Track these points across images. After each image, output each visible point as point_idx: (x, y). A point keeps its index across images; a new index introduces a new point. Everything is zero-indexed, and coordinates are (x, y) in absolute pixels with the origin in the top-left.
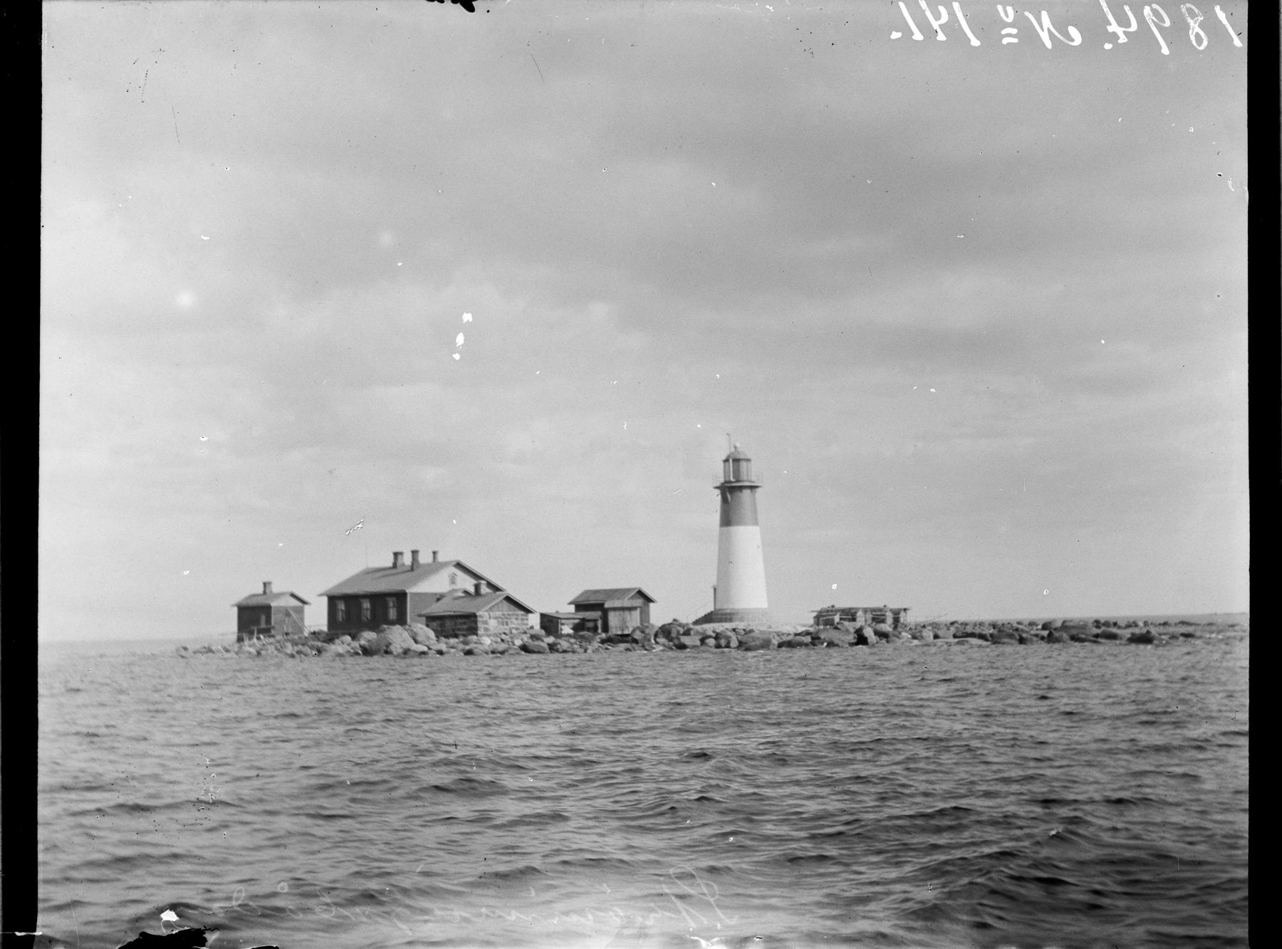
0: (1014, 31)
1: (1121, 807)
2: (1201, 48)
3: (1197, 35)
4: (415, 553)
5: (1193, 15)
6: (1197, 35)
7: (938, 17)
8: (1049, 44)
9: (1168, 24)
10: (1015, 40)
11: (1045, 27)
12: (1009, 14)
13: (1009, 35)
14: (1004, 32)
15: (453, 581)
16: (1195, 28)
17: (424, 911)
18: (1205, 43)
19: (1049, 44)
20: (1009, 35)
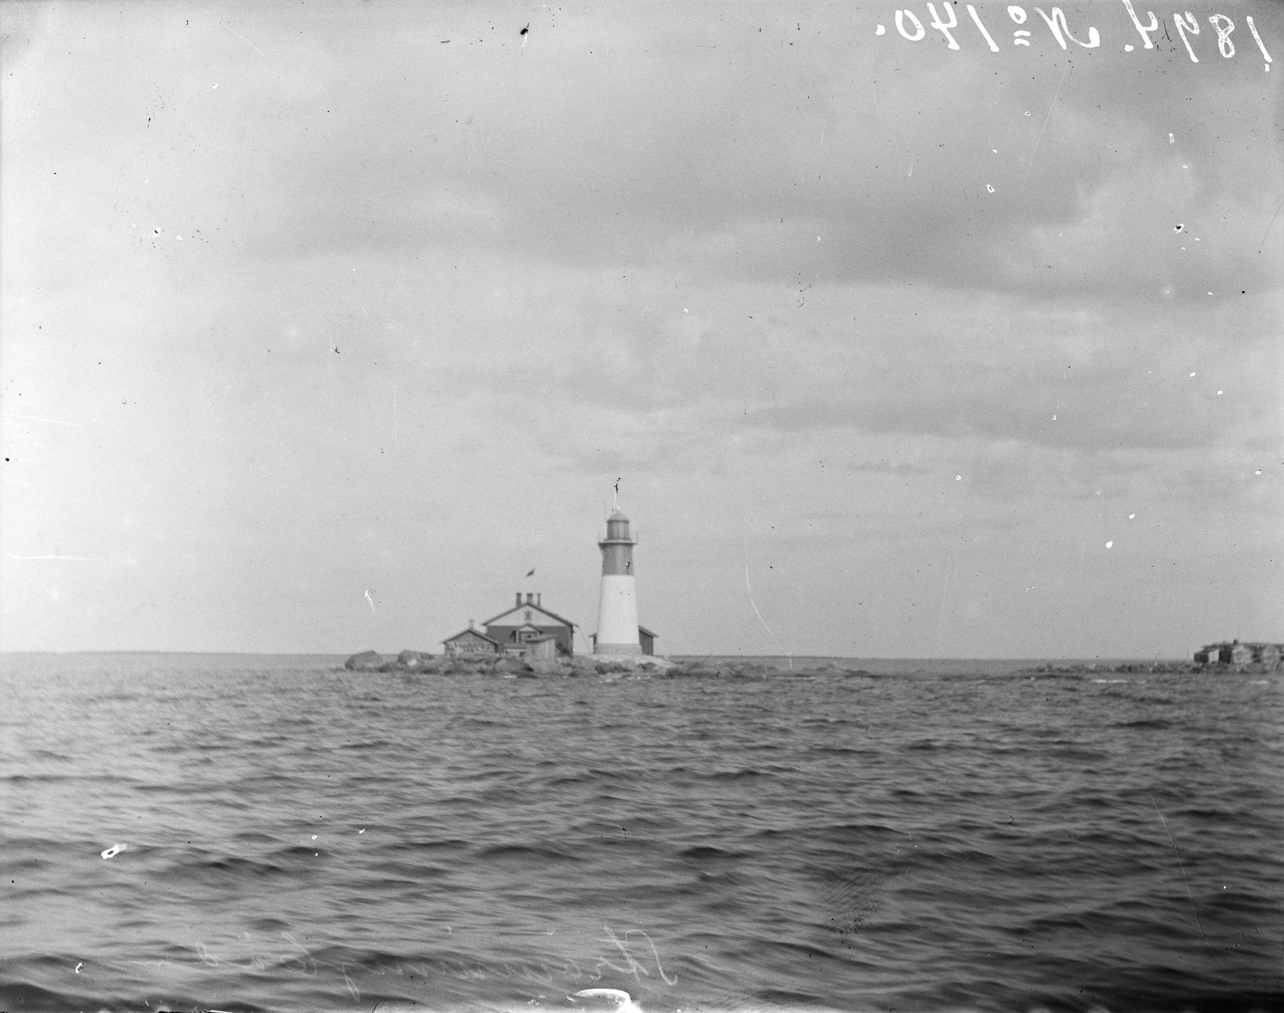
0: (1028, 34)
1: (228, 877)
2: (1229, 56)
3: (1226, 45)
4: (530, 595)
5: (1223, 24)
6: (1226, 45)
7: (946, 20)
8: (1063, 45)
9: (1196, 32)
10: (1027, 43)
11: (1056, 23)
12: (1017, 13)
13: (1022, 37)
14: (1017, 34)
15: (528, 615)
16: (1223, 37)
17: (1210, 904)
18: (1232, 53)
19: (1063, 45)
20: (1022, 37)
